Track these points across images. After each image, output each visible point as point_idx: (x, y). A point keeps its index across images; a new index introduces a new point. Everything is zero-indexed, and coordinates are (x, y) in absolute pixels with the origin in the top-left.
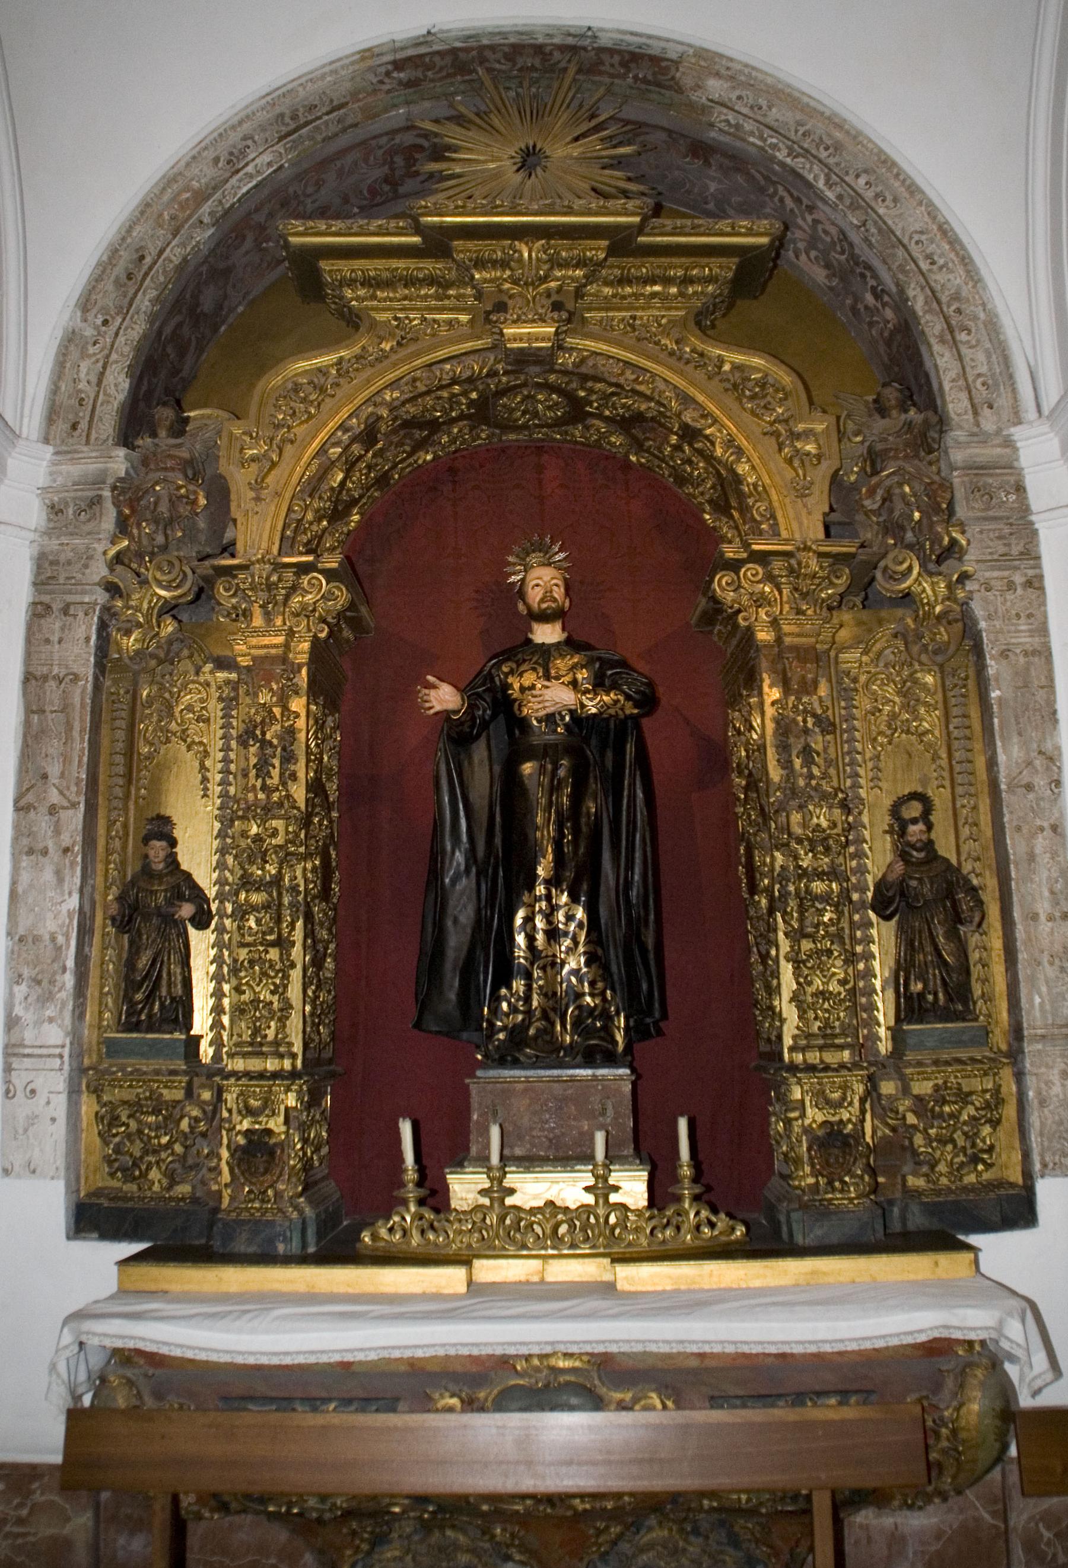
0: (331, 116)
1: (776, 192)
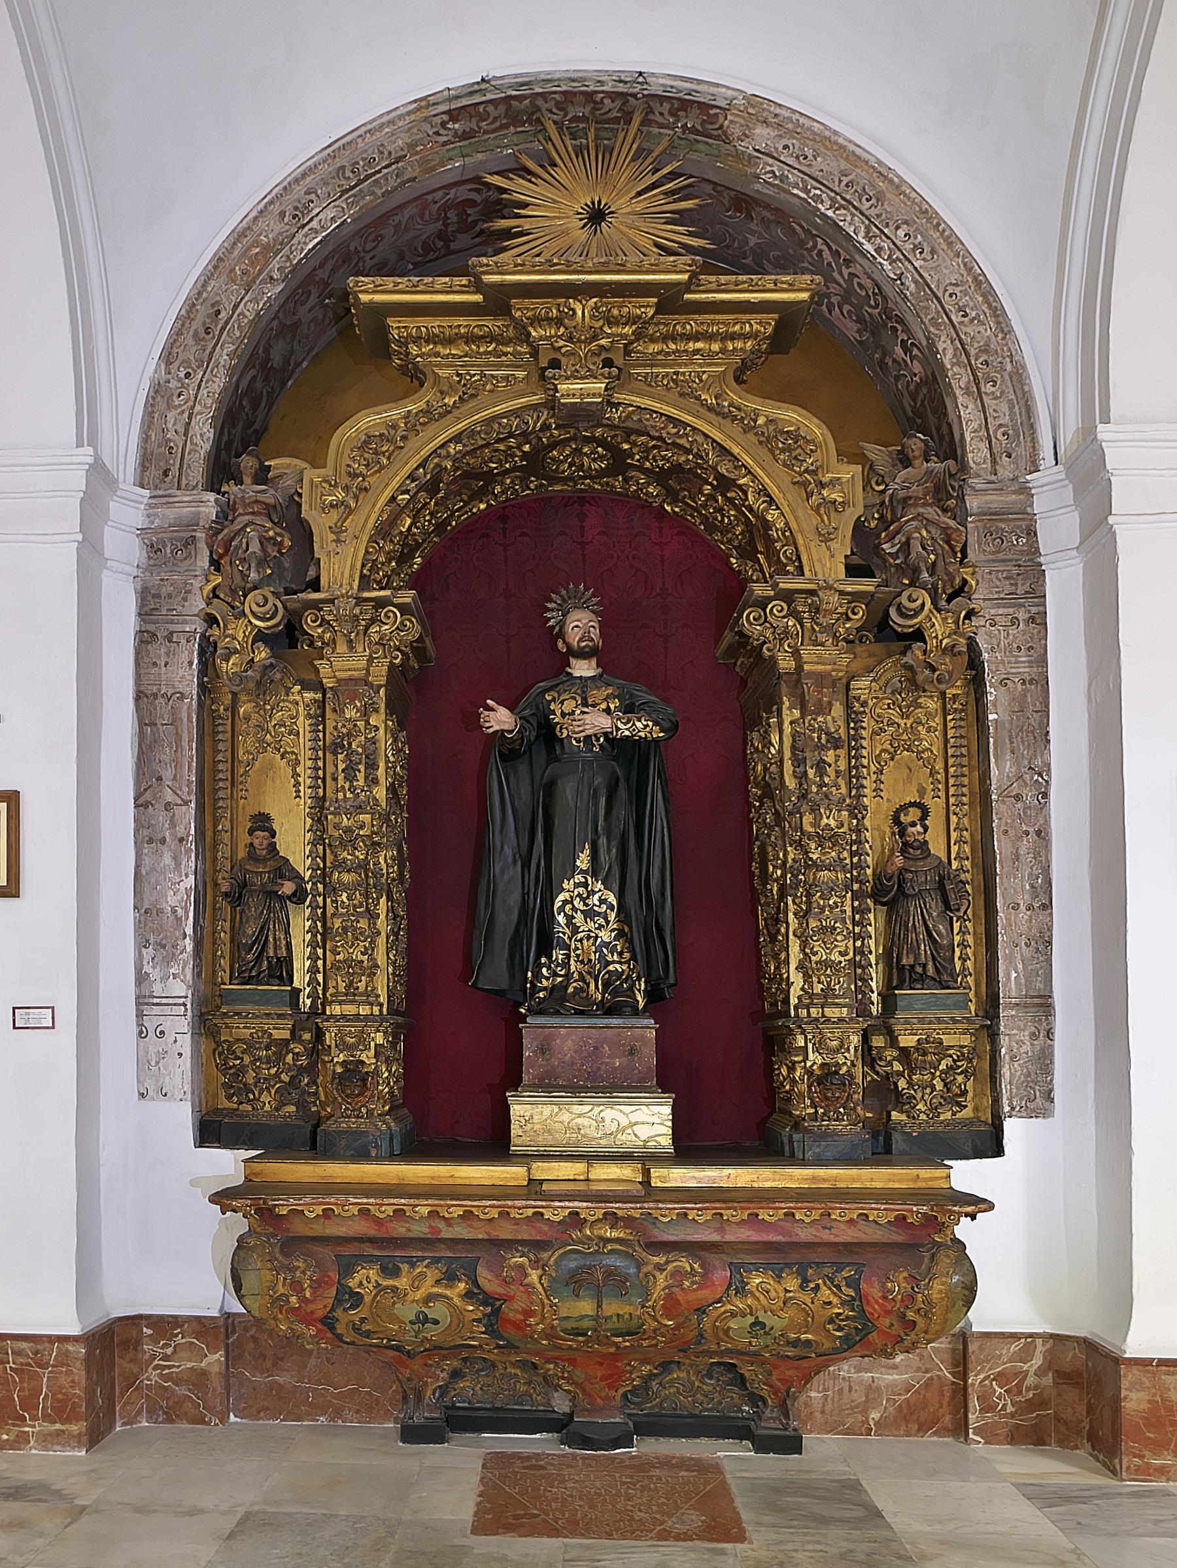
0: (390, 169)
1: (815, 246)
